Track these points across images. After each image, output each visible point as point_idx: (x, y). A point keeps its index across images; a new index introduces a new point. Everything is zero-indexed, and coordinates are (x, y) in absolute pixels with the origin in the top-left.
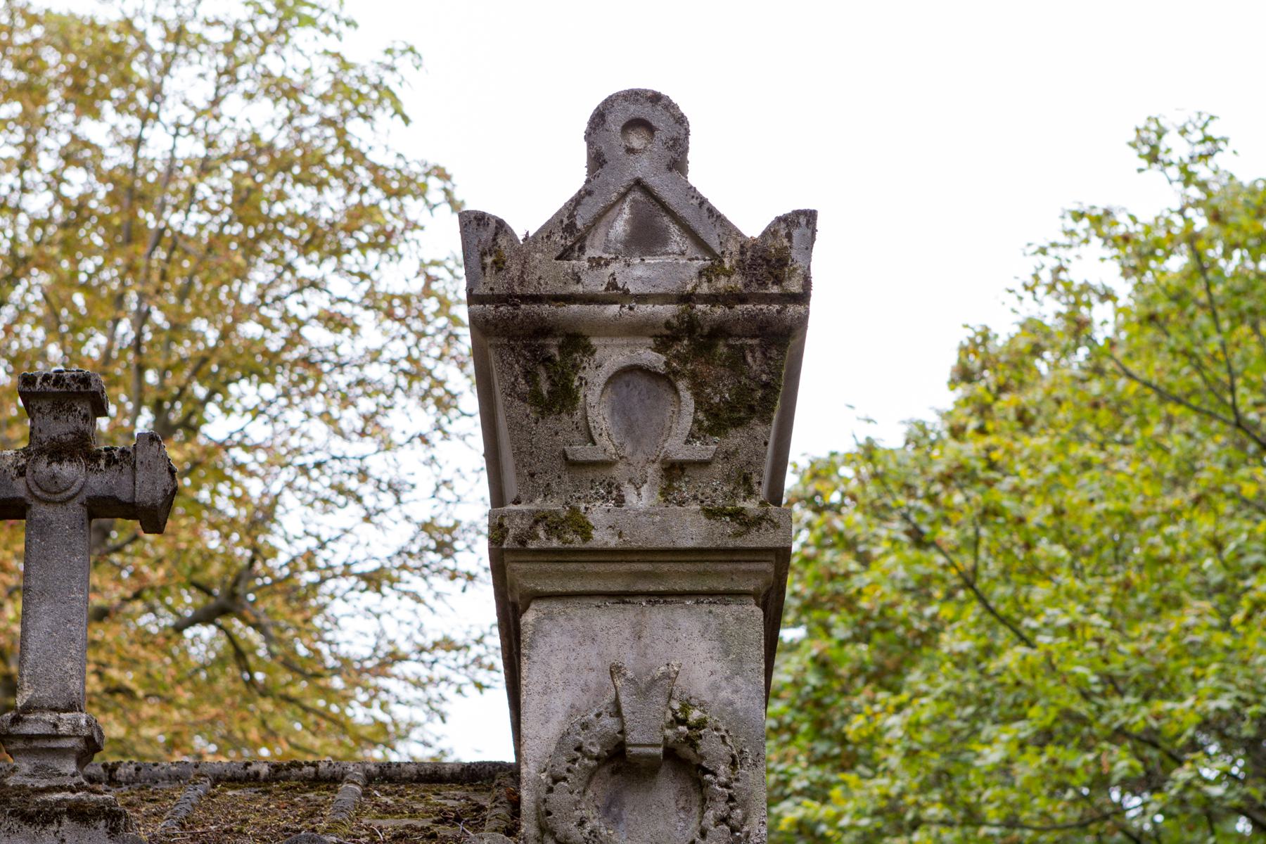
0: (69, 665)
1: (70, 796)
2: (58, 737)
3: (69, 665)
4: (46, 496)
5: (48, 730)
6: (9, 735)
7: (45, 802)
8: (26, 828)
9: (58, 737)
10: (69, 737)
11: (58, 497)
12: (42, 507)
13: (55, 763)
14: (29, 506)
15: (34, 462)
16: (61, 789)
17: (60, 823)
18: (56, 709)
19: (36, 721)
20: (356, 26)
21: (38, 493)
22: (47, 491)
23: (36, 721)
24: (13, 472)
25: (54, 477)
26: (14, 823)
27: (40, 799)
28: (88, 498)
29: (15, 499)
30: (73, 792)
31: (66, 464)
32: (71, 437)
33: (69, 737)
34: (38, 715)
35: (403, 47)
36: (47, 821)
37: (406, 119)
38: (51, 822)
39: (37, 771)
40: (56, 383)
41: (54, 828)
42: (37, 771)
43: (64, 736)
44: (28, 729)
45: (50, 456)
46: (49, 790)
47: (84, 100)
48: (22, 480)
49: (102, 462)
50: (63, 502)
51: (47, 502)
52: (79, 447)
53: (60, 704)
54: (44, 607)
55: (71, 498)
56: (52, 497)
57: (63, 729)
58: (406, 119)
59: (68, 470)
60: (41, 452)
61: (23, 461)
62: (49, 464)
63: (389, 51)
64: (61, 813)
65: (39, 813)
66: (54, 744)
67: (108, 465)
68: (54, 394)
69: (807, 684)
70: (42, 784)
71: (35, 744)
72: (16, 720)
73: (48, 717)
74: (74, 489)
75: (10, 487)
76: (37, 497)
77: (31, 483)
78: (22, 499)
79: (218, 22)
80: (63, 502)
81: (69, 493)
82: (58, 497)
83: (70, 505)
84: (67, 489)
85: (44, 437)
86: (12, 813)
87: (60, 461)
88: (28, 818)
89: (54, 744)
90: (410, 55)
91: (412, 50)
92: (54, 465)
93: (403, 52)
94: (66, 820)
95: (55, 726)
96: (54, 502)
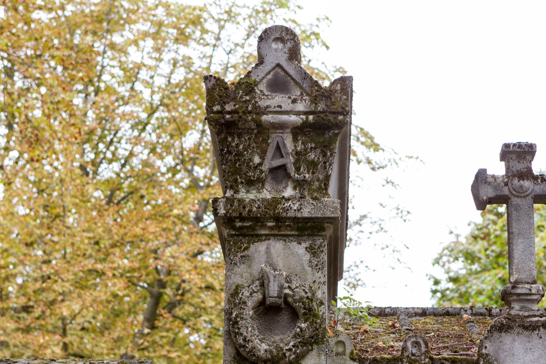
0: (532, 265)
1: (540, 319)
2: (531, 294)
3: (532, 265)
4: (518, 194)
5: (527, 291)
6: (511, 293)
7: (531, 321)
8: (525, 332)
9: (531, 294)
10: (536, 294)
11: (523, 195)
12: (516, 199)
13: (529, 305)
14: (510, 198)
15: (512, 180)
16: (535, 316)
17: (539, 330)
18: (528, 283)
19: (522, 288)
20: (302, 8)
21: (514, 193)
22: (518, 192)
23: (522, 288)
24: (503, 184)
25: (521, 186)
26: (520, 330)
27: (529, 320)
28: (535, 195)
29: (504, 195)
30: (541, 317)
31: (526, 181)
32: (525, 170)
33: (536, 294)
34: (522, 285)
35: (324, 17)
36: (534, 329)
37: (327, 47)
38: (536, 330)
39: (522, 308)
40: (519, 147)
41: (537, 332)
42: (522, 308)
43: (533, 294)
44: (519, 291)
45: (519, 178)
46: (529, 316)
47: (183, 38)
48: (506, 188)
49: (539, 180)
50: (525, 197)
51: (518, 197)
52: (528, 174)
53: (530, 281)
54: (520, 241)
55: (528, 195)
56: (520, 195)
57: (534, 291)
58: (327, 47)
59: (527, 184)
60: (514, 176)
61: (506, 180)
62: (519, 181)
63: (318, 19)
64: (539, 326)
65: (530, 326)
66: (529, 297)
67: (542, 181)
68: (518, 151)
69: (497, 289)
70: (526, 314)
71: (521, 297)
72: (514, 287)
73: (527, 286)
74: (529, 192)
75: (502, 190)
76: (513, 195)
77: (511, 189)
78: (507, 195)
79: (244, 6)
80: (525, 197)
81: (527, 193)
82: (523, 195)
83: (527, 198)
84: (526, 191)
85: (514, 169)
86: (519, 326)
87: (523, 180)
88: (526, 328)
89: (529, 297)
90: (326, 20)
91: (328, 19)
92: (521, 181)
93: (324, 19)
94: (542, 329)
95: (530, 290)
96: (521, 197)
